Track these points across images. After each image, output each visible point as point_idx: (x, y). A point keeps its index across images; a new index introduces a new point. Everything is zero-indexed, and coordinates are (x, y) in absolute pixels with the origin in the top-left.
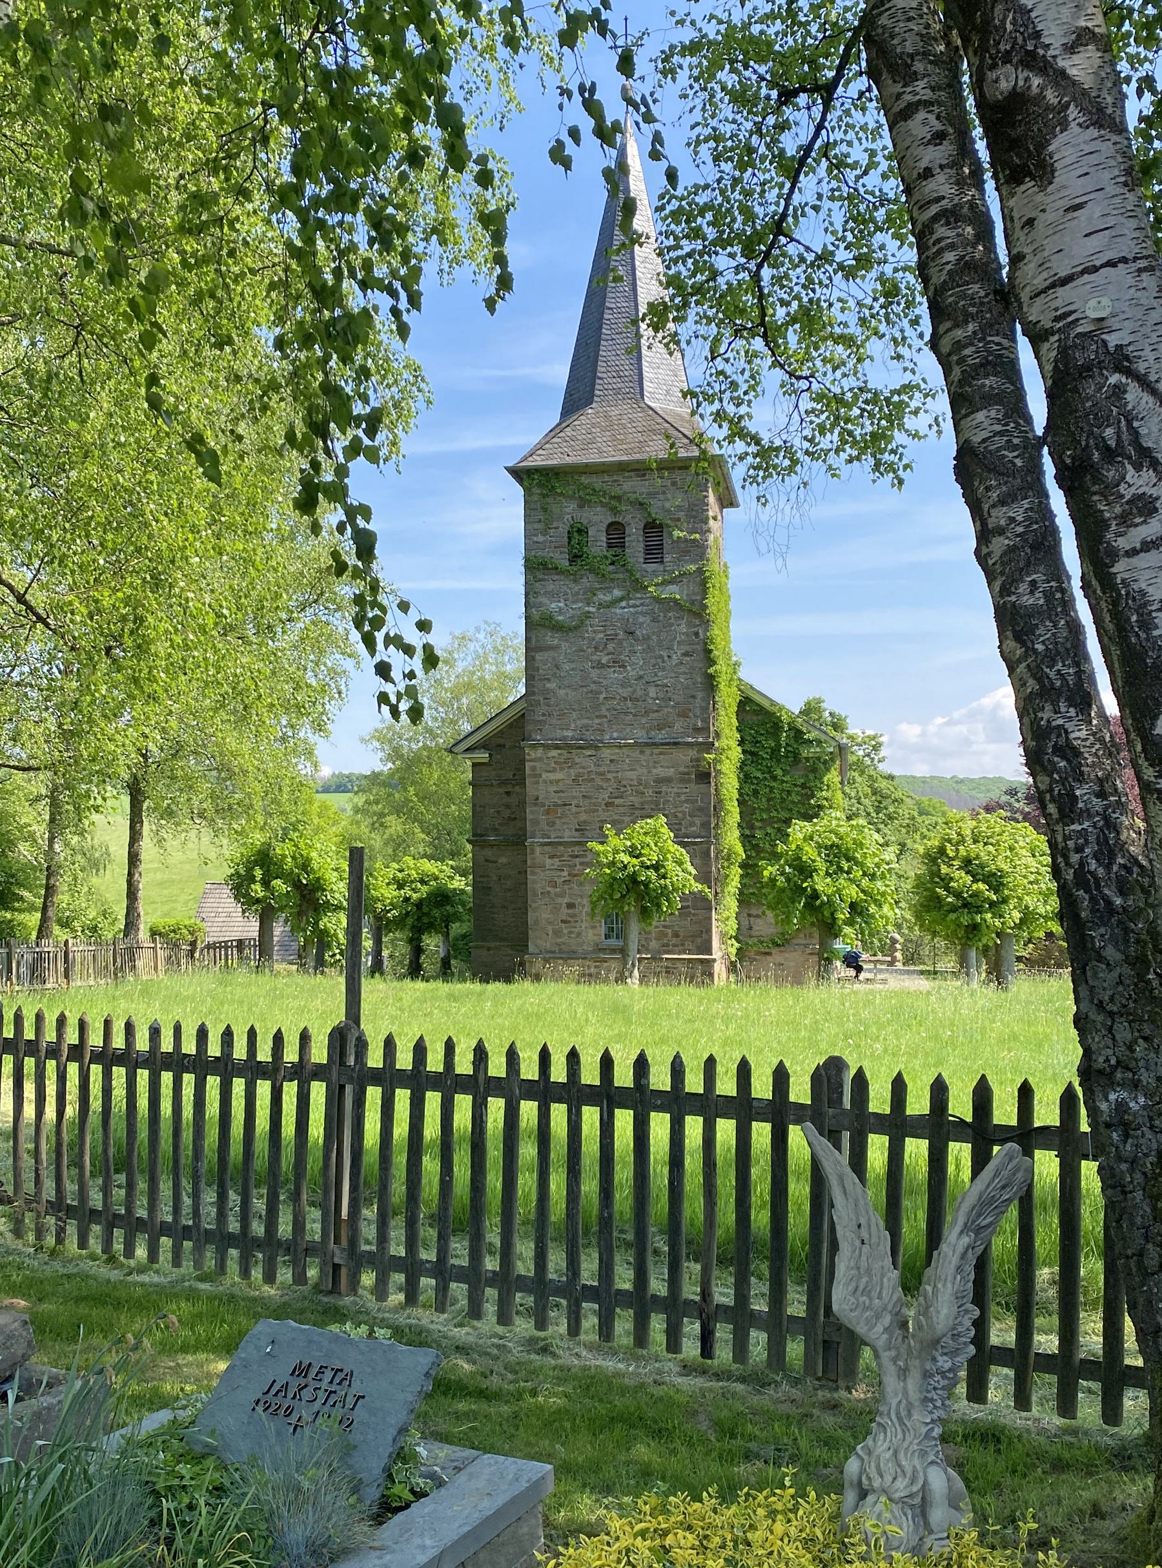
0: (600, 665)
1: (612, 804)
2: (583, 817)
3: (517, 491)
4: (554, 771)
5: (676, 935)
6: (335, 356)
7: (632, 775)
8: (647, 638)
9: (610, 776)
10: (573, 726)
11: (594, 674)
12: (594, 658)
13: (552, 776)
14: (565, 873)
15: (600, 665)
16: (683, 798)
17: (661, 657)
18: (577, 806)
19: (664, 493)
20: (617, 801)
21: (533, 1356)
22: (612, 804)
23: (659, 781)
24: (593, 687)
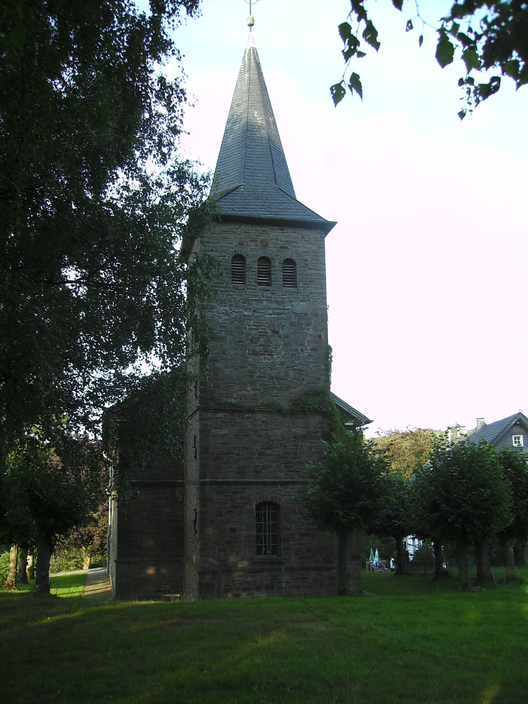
0: (255, 353)
1: (263, 454)
2: (242, 463)
3: (329, 219)
4: (220, 428)
5: (309, 551)
6: (51, 18)
7: (278, 433)
8: (286, 336)
9: (262, 433)
10: (235, 395)
11: (250, 359)
12: (251, 347)
13: (220, 432)
14: (228, 506)
15: (255, 353)
16: (313, 450)
17: (296, 350)
18: (238, 455)
19: (296, 242)
20: (268, 452)
21: (63, 155)
22: (263, 454)
23: (296, 437)
24: (249, 368)
